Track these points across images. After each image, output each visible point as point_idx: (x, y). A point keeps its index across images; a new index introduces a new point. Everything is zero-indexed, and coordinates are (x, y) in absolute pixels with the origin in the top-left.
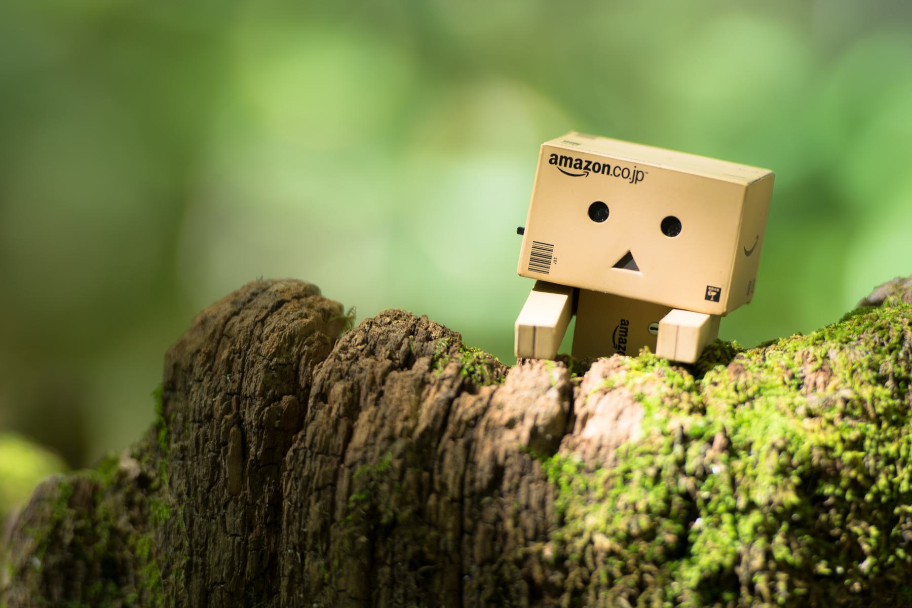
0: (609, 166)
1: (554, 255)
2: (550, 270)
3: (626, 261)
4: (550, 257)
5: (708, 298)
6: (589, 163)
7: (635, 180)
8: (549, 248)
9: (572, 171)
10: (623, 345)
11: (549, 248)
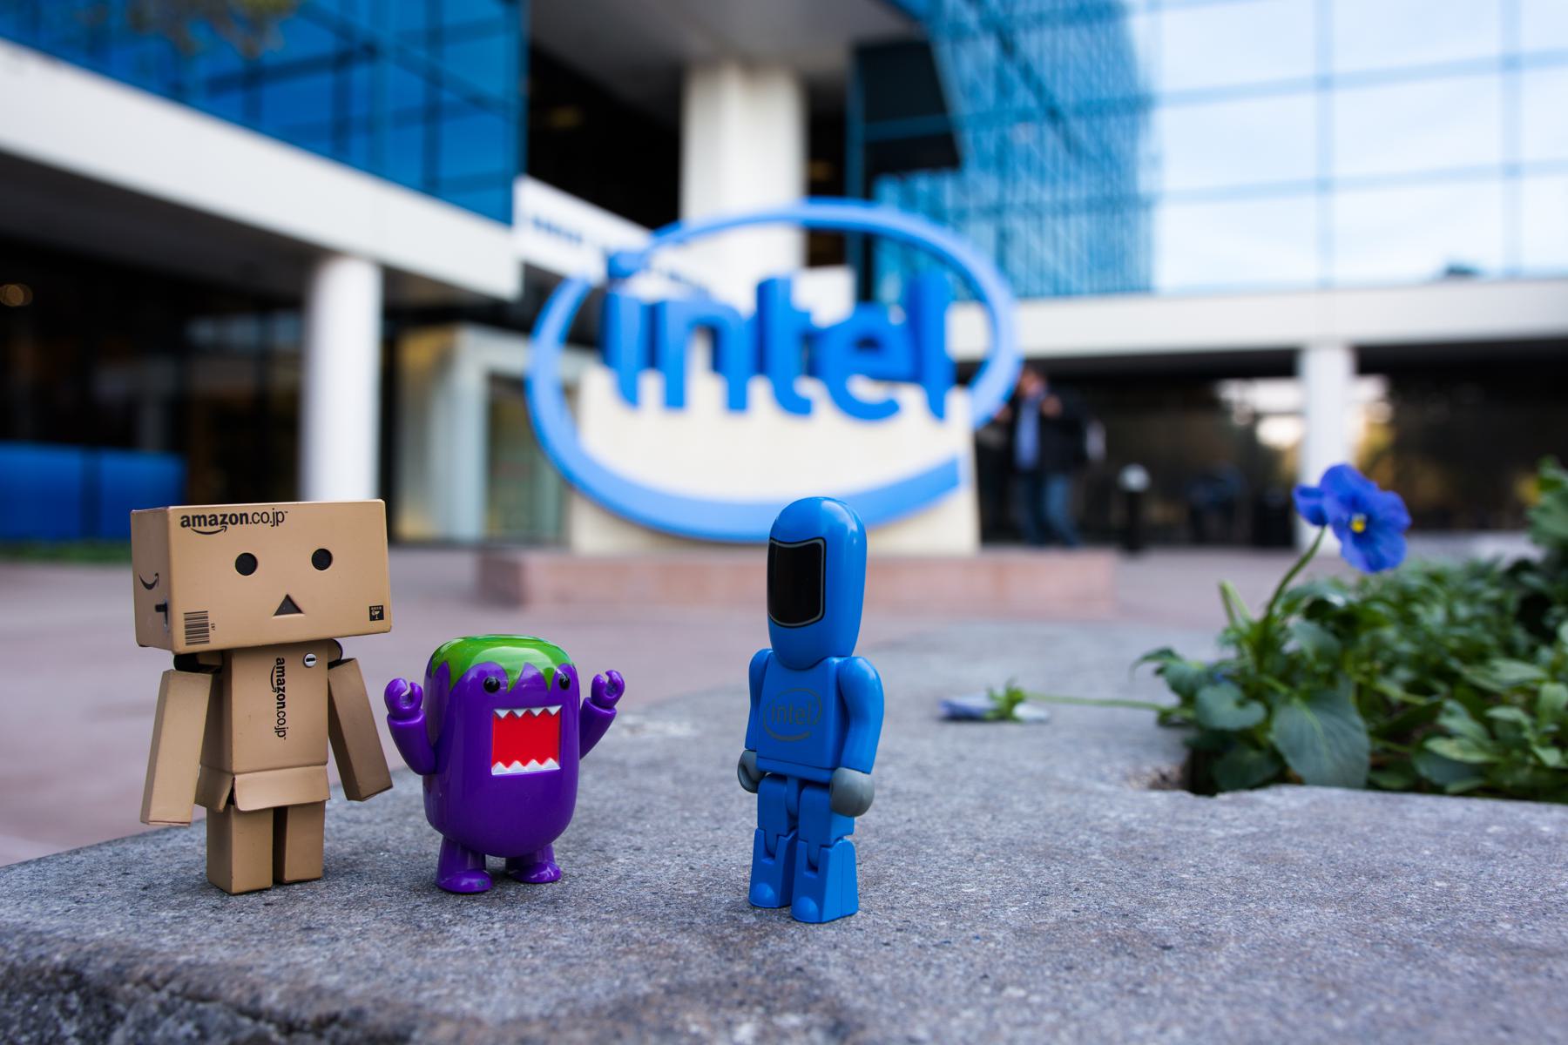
1: (210, 621)
3: (289, 606)
5: (373, 618)
8: (204, 615)
9: (209, 529)
11: (204, 615)
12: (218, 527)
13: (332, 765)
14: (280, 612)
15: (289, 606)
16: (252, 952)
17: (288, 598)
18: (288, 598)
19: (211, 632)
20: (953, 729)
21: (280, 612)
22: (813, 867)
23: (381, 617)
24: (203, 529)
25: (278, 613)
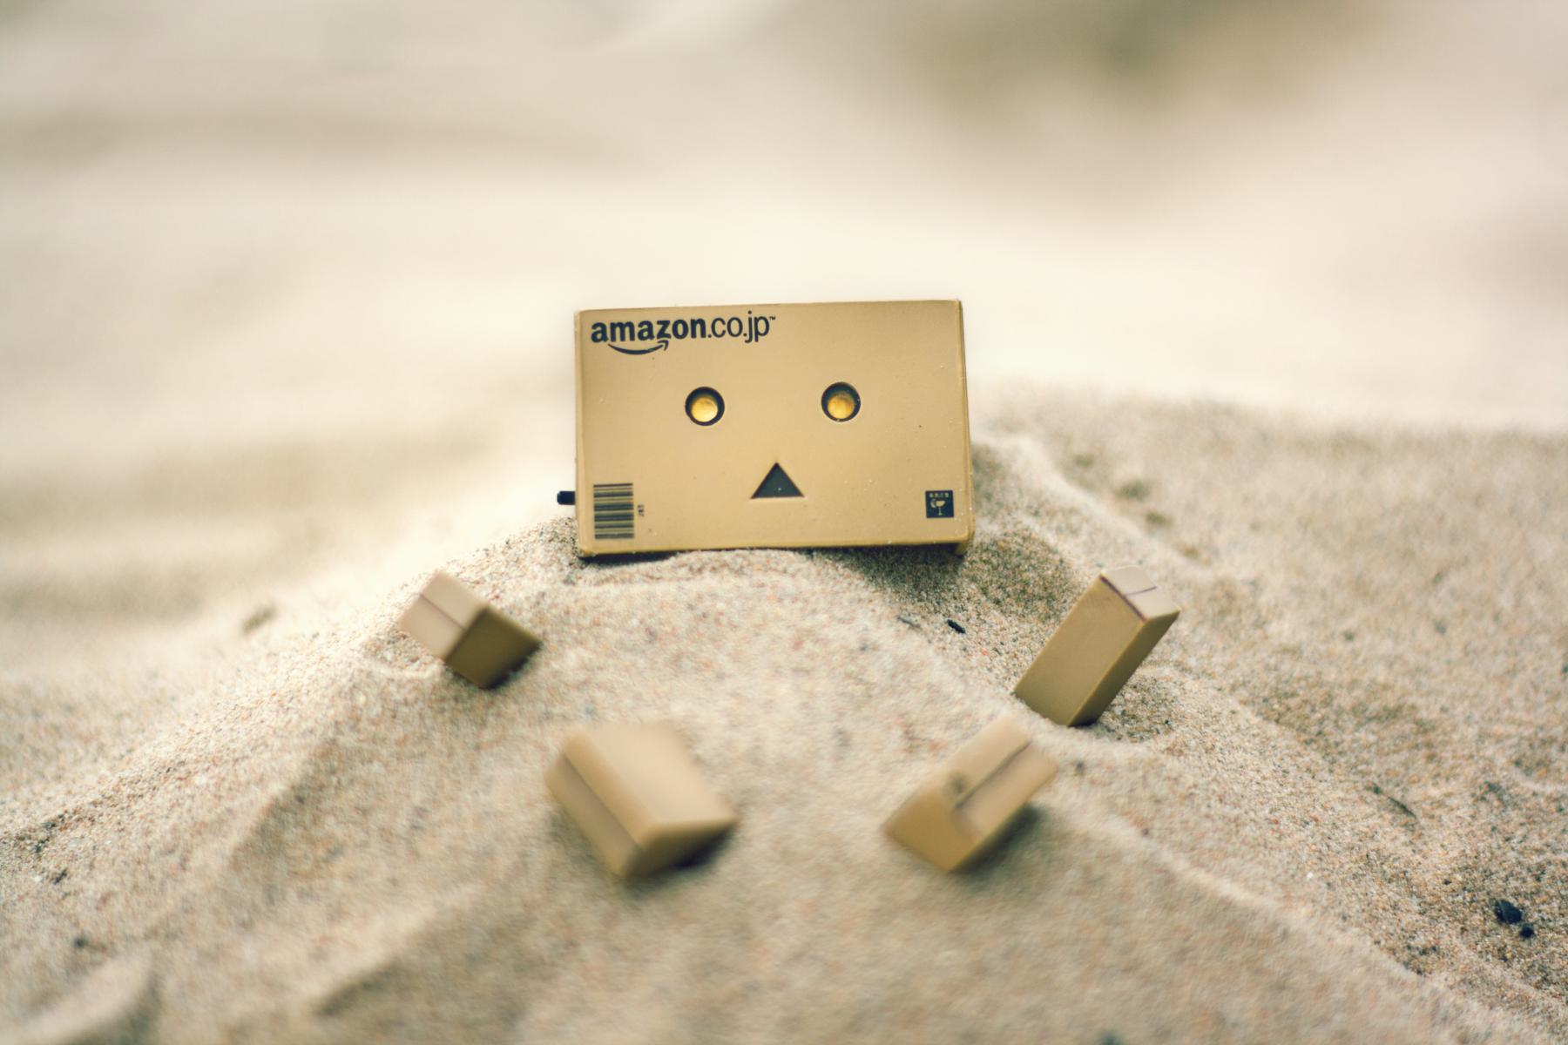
0: (702, 322)
1: (637, 500)
2: (637, 530)
4: (629, 506)
5: (932, 513)
6: (665, 324)
7: (755, 335)
8: (625, 490)
9: (638, 344)
10: (656, 329)
11: (625, 490)
12: (653, 343)
13: (1143, 673)
14: (763, 491)
15: (776, 483)
16: (1400, 682)
17: (776, 467)
18: (776, 467)
19: (637, 520)
20: (591, 573)
21: (763, 491)
22: (1405, 825)
23: (948, 511)
24: (618, 343)
25: (757, 495)
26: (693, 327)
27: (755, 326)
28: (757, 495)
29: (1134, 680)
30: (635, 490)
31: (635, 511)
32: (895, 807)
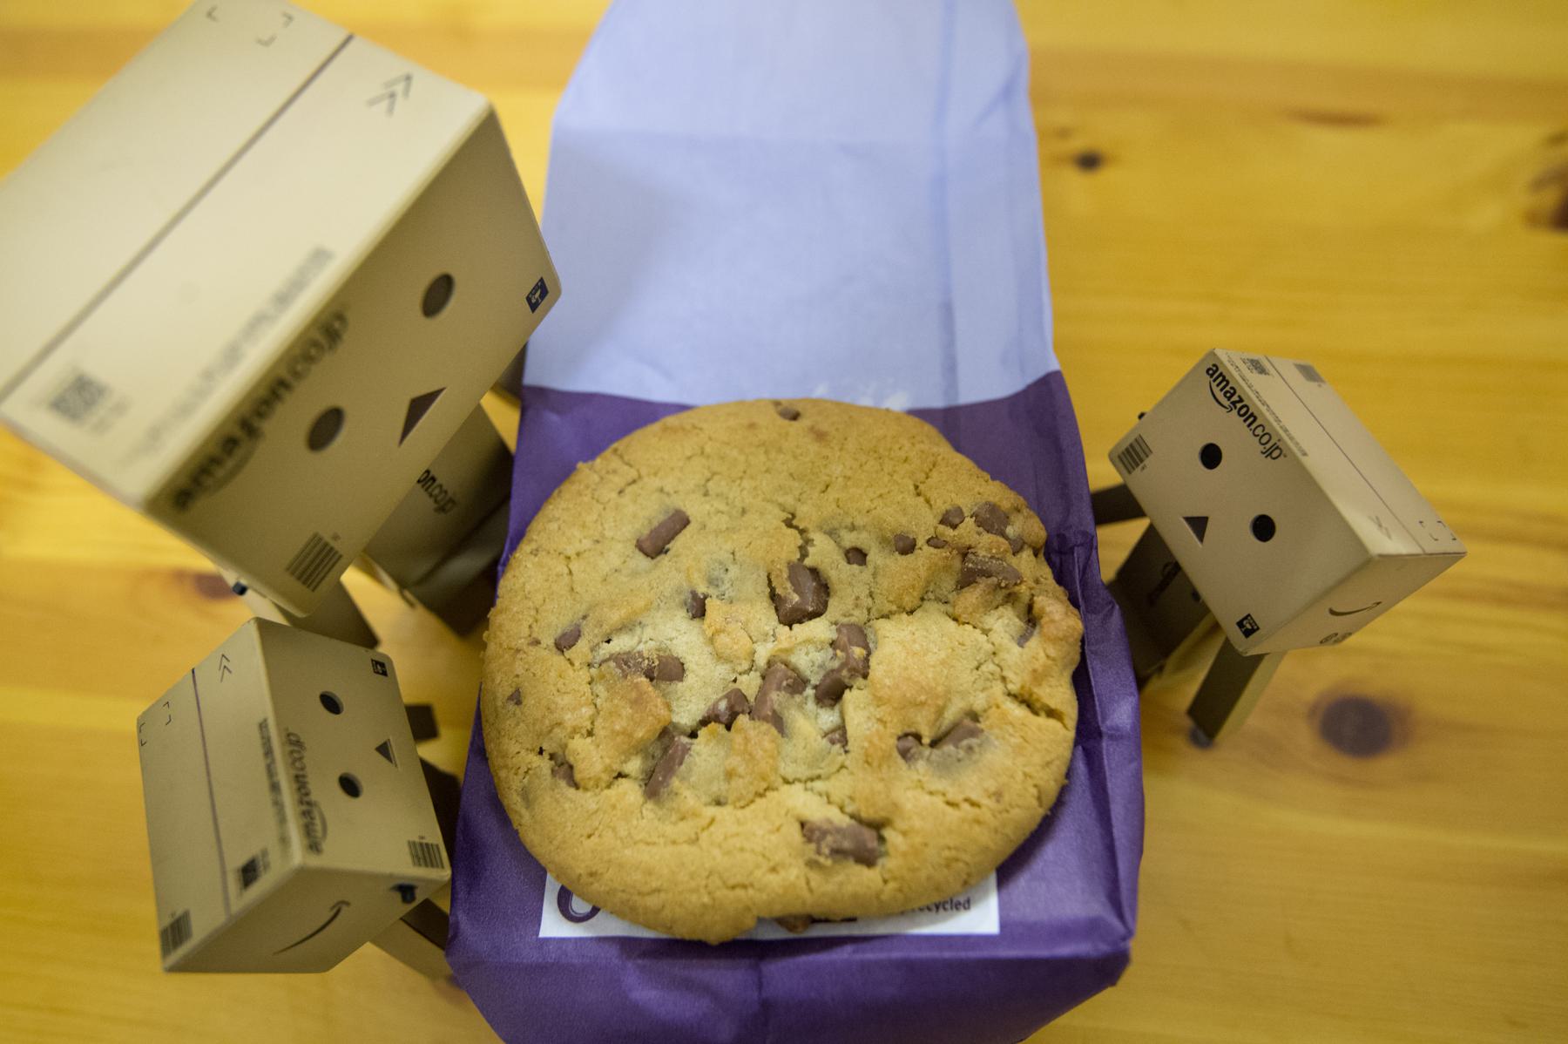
1: (1147, 462)
4: (326, 544)
5: (1240, 624)
6: (1241, 400)
7: (1268, 453)
9: (1220, 396)
10: (1235, 398)
12: (1226, 403)
19: (1138, 470)
23: (1248, 633)
25: (1187, 519)
26: (1249, 417)
27: (1273, 449)
28: (1187, 519)
29: (1416, 550)
30: (1151, 457)
31: (332, 543)
32: (715, 962)
